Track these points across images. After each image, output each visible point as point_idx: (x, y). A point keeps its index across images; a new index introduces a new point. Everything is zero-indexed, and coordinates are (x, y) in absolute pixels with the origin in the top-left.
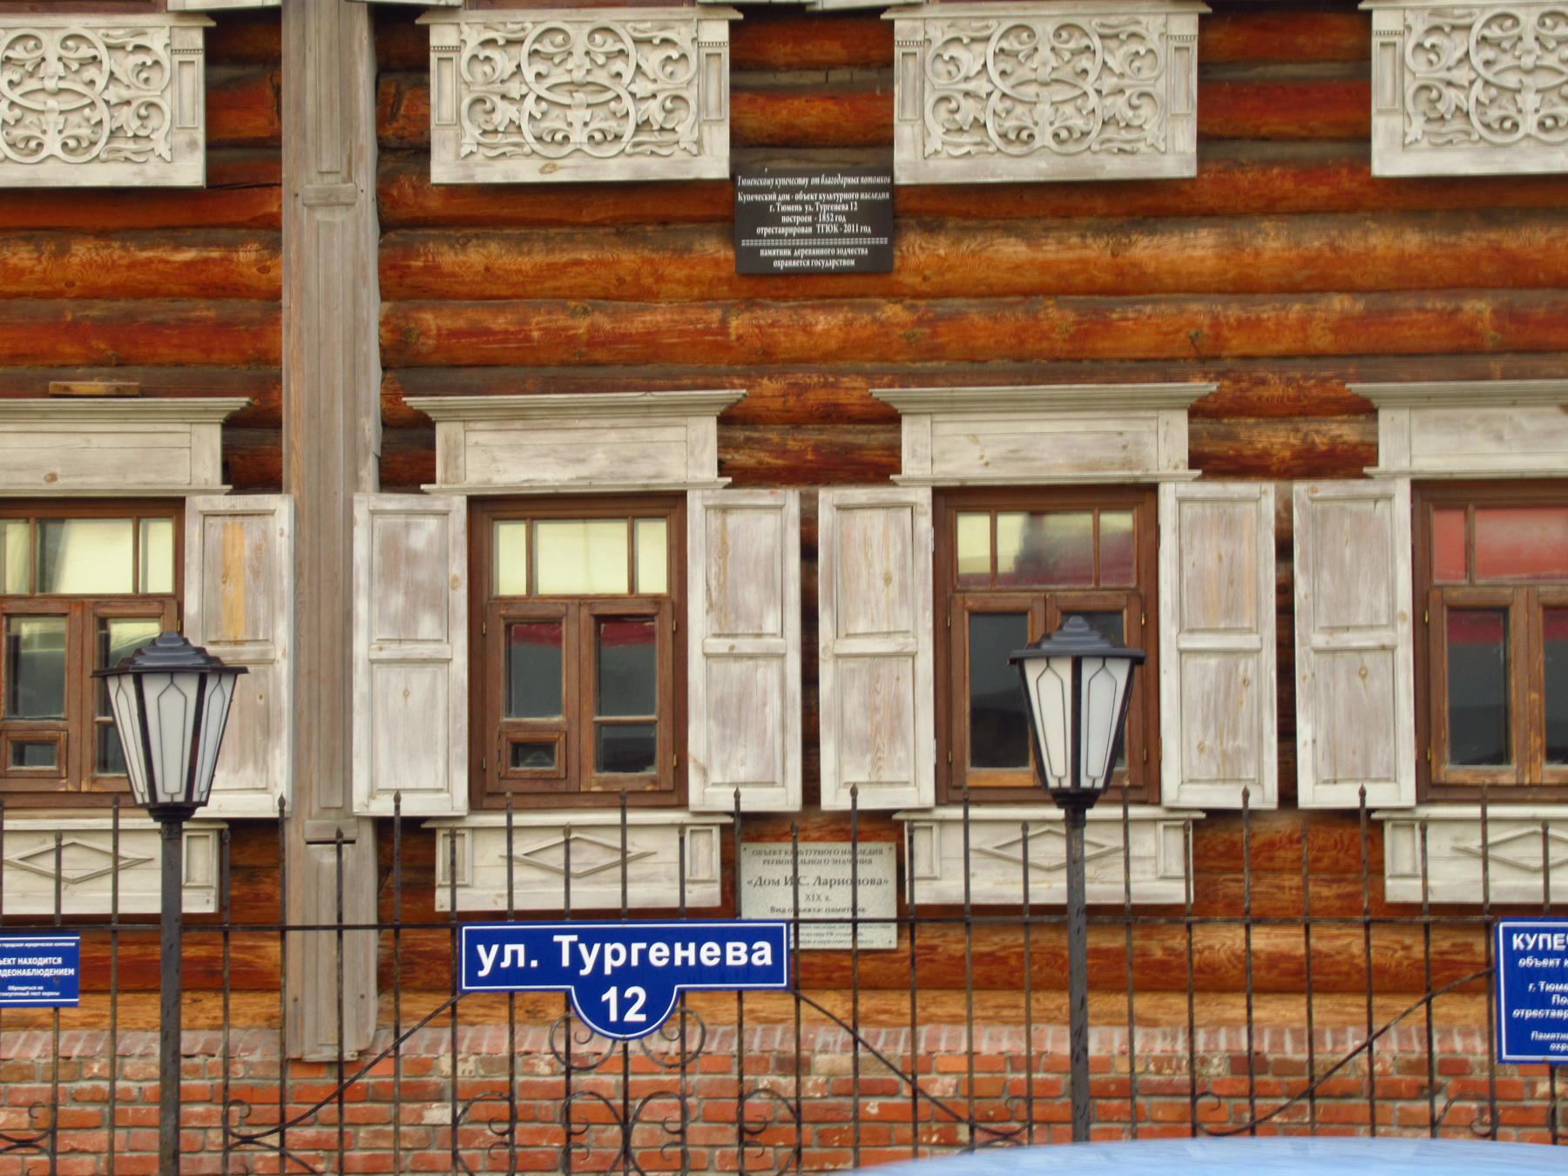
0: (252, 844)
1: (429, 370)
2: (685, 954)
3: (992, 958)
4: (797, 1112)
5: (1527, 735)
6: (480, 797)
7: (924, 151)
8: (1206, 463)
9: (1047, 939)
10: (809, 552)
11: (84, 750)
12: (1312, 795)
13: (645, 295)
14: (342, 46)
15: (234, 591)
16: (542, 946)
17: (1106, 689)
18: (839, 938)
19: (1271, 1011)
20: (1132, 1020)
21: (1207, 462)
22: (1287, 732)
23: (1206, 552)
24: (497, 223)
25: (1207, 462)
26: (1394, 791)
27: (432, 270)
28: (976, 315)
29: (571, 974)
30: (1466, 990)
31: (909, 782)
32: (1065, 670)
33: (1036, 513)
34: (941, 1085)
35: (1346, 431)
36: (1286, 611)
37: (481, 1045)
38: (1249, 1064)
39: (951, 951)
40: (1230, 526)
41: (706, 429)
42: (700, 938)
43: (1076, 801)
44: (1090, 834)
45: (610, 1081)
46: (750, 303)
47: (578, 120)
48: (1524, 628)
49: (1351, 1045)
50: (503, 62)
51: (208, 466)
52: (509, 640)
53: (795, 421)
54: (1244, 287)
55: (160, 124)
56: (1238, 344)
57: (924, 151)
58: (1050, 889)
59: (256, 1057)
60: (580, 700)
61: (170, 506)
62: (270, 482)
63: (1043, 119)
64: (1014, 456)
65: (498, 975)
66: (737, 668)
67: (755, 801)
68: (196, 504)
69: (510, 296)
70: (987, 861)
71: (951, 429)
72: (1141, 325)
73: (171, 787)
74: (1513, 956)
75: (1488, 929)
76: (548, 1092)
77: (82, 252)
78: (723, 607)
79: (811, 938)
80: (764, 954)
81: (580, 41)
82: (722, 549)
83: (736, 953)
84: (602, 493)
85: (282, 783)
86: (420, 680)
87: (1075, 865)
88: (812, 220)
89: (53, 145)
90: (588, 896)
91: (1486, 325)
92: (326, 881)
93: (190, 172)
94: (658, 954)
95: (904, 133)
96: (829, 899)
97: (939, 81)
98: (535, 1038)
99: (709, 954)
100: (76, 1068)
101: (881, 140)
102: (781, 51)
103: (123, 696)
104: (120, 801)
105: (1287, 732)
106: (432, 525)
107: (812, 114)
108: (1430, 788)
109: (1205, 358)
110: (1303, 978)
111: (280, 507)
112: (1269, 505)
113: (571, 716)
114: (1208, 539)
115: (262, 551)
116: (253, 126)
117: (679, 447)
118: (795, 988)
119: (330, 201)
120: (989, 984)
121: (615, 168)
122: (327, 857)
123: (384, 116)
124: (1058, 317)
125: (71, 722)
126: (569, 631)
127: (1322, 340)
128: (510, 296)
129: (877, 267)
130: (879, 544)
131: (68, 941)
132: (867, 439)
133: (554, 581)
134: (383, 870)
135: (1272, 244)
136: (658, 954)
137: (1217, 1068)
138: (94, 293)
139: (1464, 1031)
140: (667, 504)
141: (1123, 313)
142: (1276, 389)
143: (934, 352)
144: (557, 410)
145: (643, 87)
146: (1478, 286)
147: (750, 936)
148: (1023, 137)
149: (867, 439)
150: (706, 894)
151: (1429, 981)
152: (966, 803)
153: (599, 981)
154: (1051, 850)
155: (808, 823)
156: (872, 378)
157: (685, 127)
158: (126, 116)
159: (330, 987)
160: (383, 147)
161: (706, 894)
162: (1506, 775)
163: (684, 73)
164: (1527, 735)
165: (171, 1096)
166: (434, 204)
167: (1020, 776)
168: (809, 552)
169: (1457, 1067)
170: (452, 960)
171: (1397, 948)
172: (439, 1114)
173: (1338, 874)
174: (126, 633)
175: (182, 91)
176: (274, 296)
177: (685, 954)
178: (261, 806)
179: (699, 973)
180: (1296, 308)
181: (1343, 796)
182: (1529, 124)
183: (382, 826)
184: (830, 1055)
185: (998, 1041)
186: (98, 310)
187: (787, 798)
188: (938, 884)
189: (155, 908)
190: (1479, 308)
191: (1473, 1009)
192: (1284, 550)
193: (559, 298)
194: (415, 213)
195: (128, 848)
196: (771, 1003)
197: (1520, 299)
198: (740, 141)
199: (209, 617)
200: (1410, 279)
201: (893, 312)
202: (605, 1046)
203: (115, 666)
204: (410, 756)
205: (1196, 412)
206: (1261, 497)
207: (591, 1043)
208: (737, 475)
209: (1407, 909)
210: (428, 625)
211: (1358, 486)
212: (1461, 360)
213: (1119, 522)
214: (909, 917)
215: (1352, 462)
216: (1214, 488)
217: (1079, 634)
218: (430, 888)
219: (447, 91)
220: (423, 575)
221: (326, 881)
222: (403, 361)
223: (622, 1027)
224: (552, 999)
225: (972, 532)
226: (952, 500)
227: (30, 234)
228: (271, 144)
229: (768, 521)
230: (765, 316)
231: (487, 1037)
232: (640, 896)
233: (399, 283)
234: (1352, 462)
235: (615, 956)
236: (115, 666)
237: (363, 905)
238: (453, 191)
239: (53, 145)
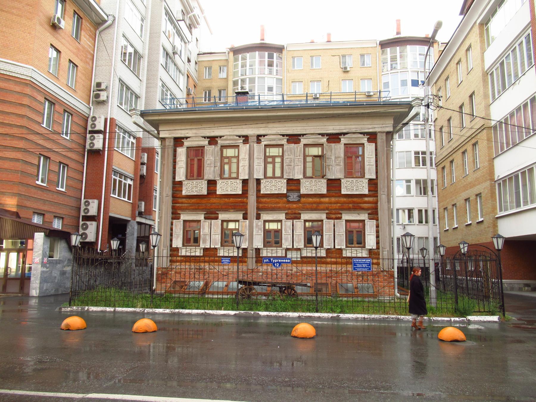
0: (245, 250)
1: (260, 209)
2: (282, 261)
5: (355, 242)
6: (264, 246)
7: (303, 191)
8: (328, 218)
9: (313, 259)
13: (279, 203)
15: (243, 228)
16: (270, 260)
17: (319, 238)
18: (296, 259)
19: (333, 266)
20: (219, 265)
21: (328, 218)
22: (334, 242)
26: (344, 247)
28: (307, 205)
31: (301, 245)
35: (339, 216)
37: (264, 268)
38: (331, 271)
39: (305, 260)
40: (329, 224)
41: (284, 215)
45: (275, 271)
47: (273, 188)
48: (355, 233)
50: (267, 183)
52: (267, 233)
53: (292, 214)
54: (331, 203)
55: (238, 189)
56: (330, 208)
57: (303, 191)
58: (314, 255)
59: (245, 268)
60: (273, 238)
61: (238, 221)
62: (247, 219)
63: (273, 188)
67: (288, 247)
69: (267, 203)
70: (308, 253)
71: (305, 215)
73: (238, 245)
77: (231, 199)
78: (285, 230)
79: (293, 259)
80: (289, 261)
82: (285, 225)
83: (287, 261)
84: (275, 220)
86: (259, 236)
87: (316, 253)
88: (293, 197)
92: (251, 254)
93: (240, 193)
94: (280, 261)
95: (301, 190)
96: (294, 256)
97: (304, 185)
98: (269, 268)
99: (284, 261)
100: (230, 269)
101: (299, 190)
102: (291, 182)
103: (234, 237)
104: (234, 246)
105: (334, 242)
106: (260, 223)
107: (293, 188)
108: (347, 247)
109: (327, 209)
110: (336, 263)
111: (247, 221)
113: (272, 239)
114: (328, 225)
115: (246, 225)
116: (246, 189)
117: (282, 216)
119: (252, 195)
121: (276, 192)
123: (257, 188)
124: (315, 205)
127: (337, 208)
128: (267, 203)
130: (299, 225)
132: (298, 216)
135: (333, 199)
136: (280, 261)
137: (328, 271)
140: (281, 221)
141: (320, 205)
142: (333, 212)
146: (351, 203)
147: (288, 259)
148: (312, 190)
150: (284, 255)
151: (347, 263)
155: (293, 249)
157: (283, 188)
159: (251, 263)
160: (257, 190)
161: (284, 255)
162: (353, 246)
164: (355, 242)
165: (238, 272)
167: (311, 245)
169: (349, 271)
171: (344, 261)
172: (261, 274)
175: (240, 186)
177: (282, 261)
178: (246, 247)
179: (283, 262)
181: (339, 247)
183: (256, 249)
184: (295, 269)
185: (309, 268)
187: (291, 247)
188: (304, 254)
190: (351, 205)
191: (350, 266)
192: (334, 226)
193: (271, 203)
194: (259, 196)
196: (290, 265)
200: (345, 203)
201: (300, 205)
203: (233, 235)
204: (258, 243)
205: (327, 214)
207: (274, 268)
208: (287, 219)
209: (345, 257)
210: (260, 231)
213: (361, 224)
214: (302, 258)
215: (340, 218)
217: (317, 233)
219: (262, 186)
221: (251, 254)
222: (258, 209)
225: (307, 224)
226: (305, 221)
227: (227, 198)
228: (247, 190)
229: (289, 223)
231: (265, 267)
232: (278, 255)
233: (258, 202)
234: (340, 218)
235: (276, 261)
236: (233, 235)
237: (254, 256)
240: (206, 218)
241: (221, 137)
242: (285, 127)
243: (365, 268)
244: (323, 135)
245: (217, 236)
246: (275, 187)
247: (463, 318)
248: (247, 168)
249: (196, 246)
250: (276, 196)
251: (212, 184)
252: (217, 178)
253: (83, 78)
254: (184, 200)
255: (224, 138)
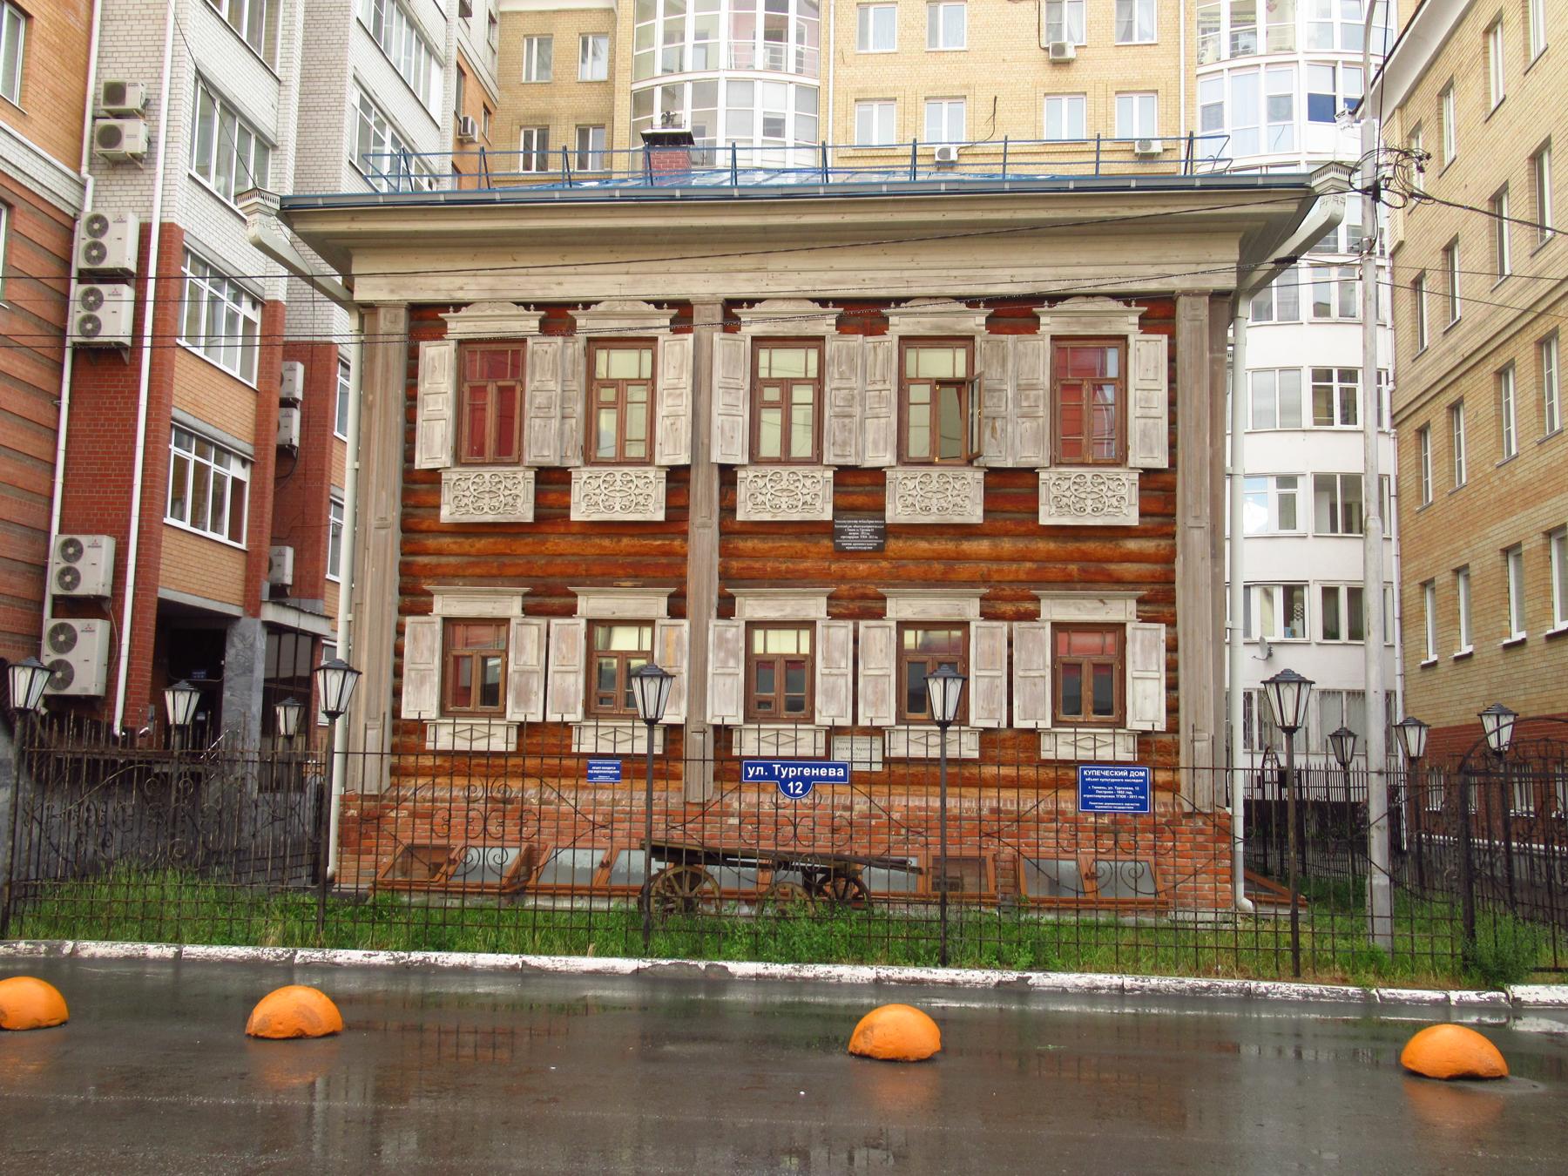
0: (674, 733)
3: (913, 775)
4: (851, 824)
6: (747, 719)
7: (896, 512)
10: (856, 641)
11: (622, 701)
12: (1017, 724)
13: (804, 557)
14: (709, 477)
15: (670, 650)
16: (769, 768)
17: (954, 688)
18: (866, 768)
19: (1006, 794)
21: (986, 615)
23: (986, 644)
24: (757, 533)
25: (986, 615)
27: (736, 548)
28: (911, 566)
29: (778, 778)
30: (1067, 788)
31: (887, 717)
32: (941, 682)
33: (926, 630)
34: (896, 816)
35: (1030, 606)
36: (1010, 664)
39: (901, 773)
40: (993, 636)
41: (823, 601)
42: (820, 767)
43: (944, 725)
44: (948, 735)
46: (838, 560)
47: (784, 501)
49: (1029, 805)
50: (760, 483)
51: (663, 610)
52: (758, 667)
53: (852, 599)
55: (651, 501)
56: (996, 577)
57: (896, 512)
58: (935, 753)
59: (675, 800)
60: (780, 688)
61: (650, 623)
62: (682, 615)
64: (923, 611)
65: (755, 777)
66: (832, 679)
67: (838, 722)
68: (659, 622)
70: (912, 744)
71: (903, 602)
72: (965, 570)
73: (651, 713)
74: (1084, 777)
75: (1076, 768)
76: (769, 815)
77: (625, 541)
79: (856, 767)
80: (841, 772)
81: (785, 476)
82: (827, 639)
83: (832, 772)
84: (789, 620)
85: (684, 715)
86: (729, 680)
87: (943, 745)
88: (858, 534)
89: (617, 507)
90: (783, 752)
91: (1075, 573)
92: (698, 745)
93: (660, 516)
94: (807, 772)
96: (860, 754)
97: (901, 491)
99: (823, 772)
102: (849, 480)
103: (636, 684)
104: (635, 717)
106: (734, 630)
107: (859, 500)
108: (1056, 722)
110: (1016, 783)
111: (685, 623)
112: (1005, 629)
113: (777, 693)
114: (986, 640)
115: (679, 638)
116: (681, 502)
117: (815, 606)
118: (851, 784)
119: (704, 526)
120: (912, 783)
121: (796, 516)
122: (700, 737)
124: (938, 567)
125: (618, 691)
126: (777, 665)
127: (1023, 576)
129: (879, 549)
130: (879, 639)
131: (617, 762)
132: (875, 605)
133: (772, 649)
134: (716, 742)
135: (1007, 545)
136: (807, 772)
137: (985, 812)
138: (629, 555)
139: (1068, 802)
140: (810, 625)
141: (958, 566)
142: (1008, 592)
143: (898, 577)
144: (775, 594)
145: (805, 491)
146: (1073, 561)
147: (836, 767)
148: (927, 509)
149: (875, 605)
150: (821, 752)
151: (1057, 785)
152: (597, 719)
153: (787, 780)
154: (935, 740)
155: (854, 730)
156: (878, 585)
157: (818, 503)
158: (641, 499)
159: (698, 781)
160: (721, 509)
161: (821, 752)
162: (1080, 718)
163: (818, 487)
164: (1087, 706)
165: (649, 812)
166: (737, 527)
168: (856, 641)
169: (1064, 813)
170: (739, 773)
172: (734, 821)
173: (1026, 750)
174: (635, 663)
175: (658, 491)
176: (685, 556)
178: (679, 720)
179: (820, 778)
180: (1014, 566)
181: (1030, 724)
182: (1089, 510)
183: (717, 728)
184: (861, 805)
185: (915, 802)
186: (629, 560)
187: (847, 721)
188: (899, 751)
189: (645, 751)
190: (1073, 567)
191: (1070, 794)
192: (1010, 644)
193: (777, 558)
194: (730, 529)
195: (637, 733)
196: (842, 788)
197: (1084, 564)
198: (835, 508)
199: (662, 658)
200: (1050, 558)
201: (884, 564)
202: (788, 801)
204: (725, 706)
206: (1003, 626)
207: (785, 800)
208: (833, 616)
210: (732, 663)
211: (1034, 624)
212: (1067, 584)
213: (957, 634)
214: (887, 761)
215: (1033, 616)
216: (988, 623)
217: (945, 670)
218: (730, 748)
219: (742, 491)
220: (730, 646)
221: (698, 745)
222: (726, 577)
223: (794, 795)
224: (771, 785)
226: (903, 625)
227: (608, 535)
228: (686, 508)
229: (842, 631)
230: (843, 565)
231: (750, 797)
232: (801, 752)
233: (725, 552)
234: (1033, 616)
235: (792, 772)
238: (743, 523)
239: (617, 507)
240: (528, 611)
241: (587, 305)
242: (832, 269)
243: (1127, 800)
244: (972, 301)
245: (571, 678)
246: (792, 496)
247: (1494, 994)
248: (685, 424)
249: (490, 716)
250: (486, 529)
251: (552, 480)
252: (574, 461)
253: (55, 63)
254: (446, 542)
255: (601, 308)
